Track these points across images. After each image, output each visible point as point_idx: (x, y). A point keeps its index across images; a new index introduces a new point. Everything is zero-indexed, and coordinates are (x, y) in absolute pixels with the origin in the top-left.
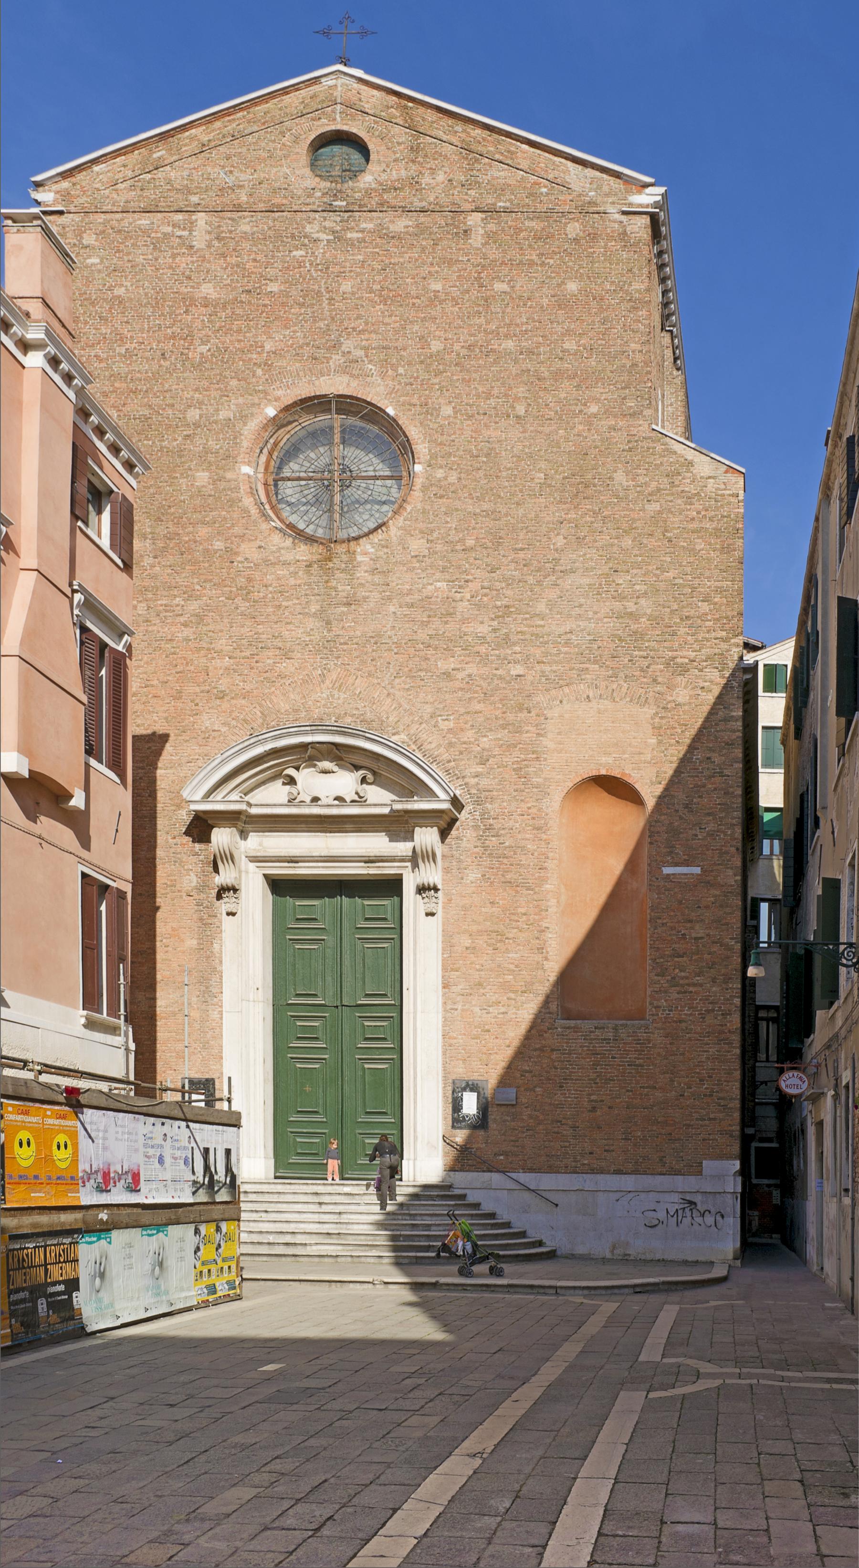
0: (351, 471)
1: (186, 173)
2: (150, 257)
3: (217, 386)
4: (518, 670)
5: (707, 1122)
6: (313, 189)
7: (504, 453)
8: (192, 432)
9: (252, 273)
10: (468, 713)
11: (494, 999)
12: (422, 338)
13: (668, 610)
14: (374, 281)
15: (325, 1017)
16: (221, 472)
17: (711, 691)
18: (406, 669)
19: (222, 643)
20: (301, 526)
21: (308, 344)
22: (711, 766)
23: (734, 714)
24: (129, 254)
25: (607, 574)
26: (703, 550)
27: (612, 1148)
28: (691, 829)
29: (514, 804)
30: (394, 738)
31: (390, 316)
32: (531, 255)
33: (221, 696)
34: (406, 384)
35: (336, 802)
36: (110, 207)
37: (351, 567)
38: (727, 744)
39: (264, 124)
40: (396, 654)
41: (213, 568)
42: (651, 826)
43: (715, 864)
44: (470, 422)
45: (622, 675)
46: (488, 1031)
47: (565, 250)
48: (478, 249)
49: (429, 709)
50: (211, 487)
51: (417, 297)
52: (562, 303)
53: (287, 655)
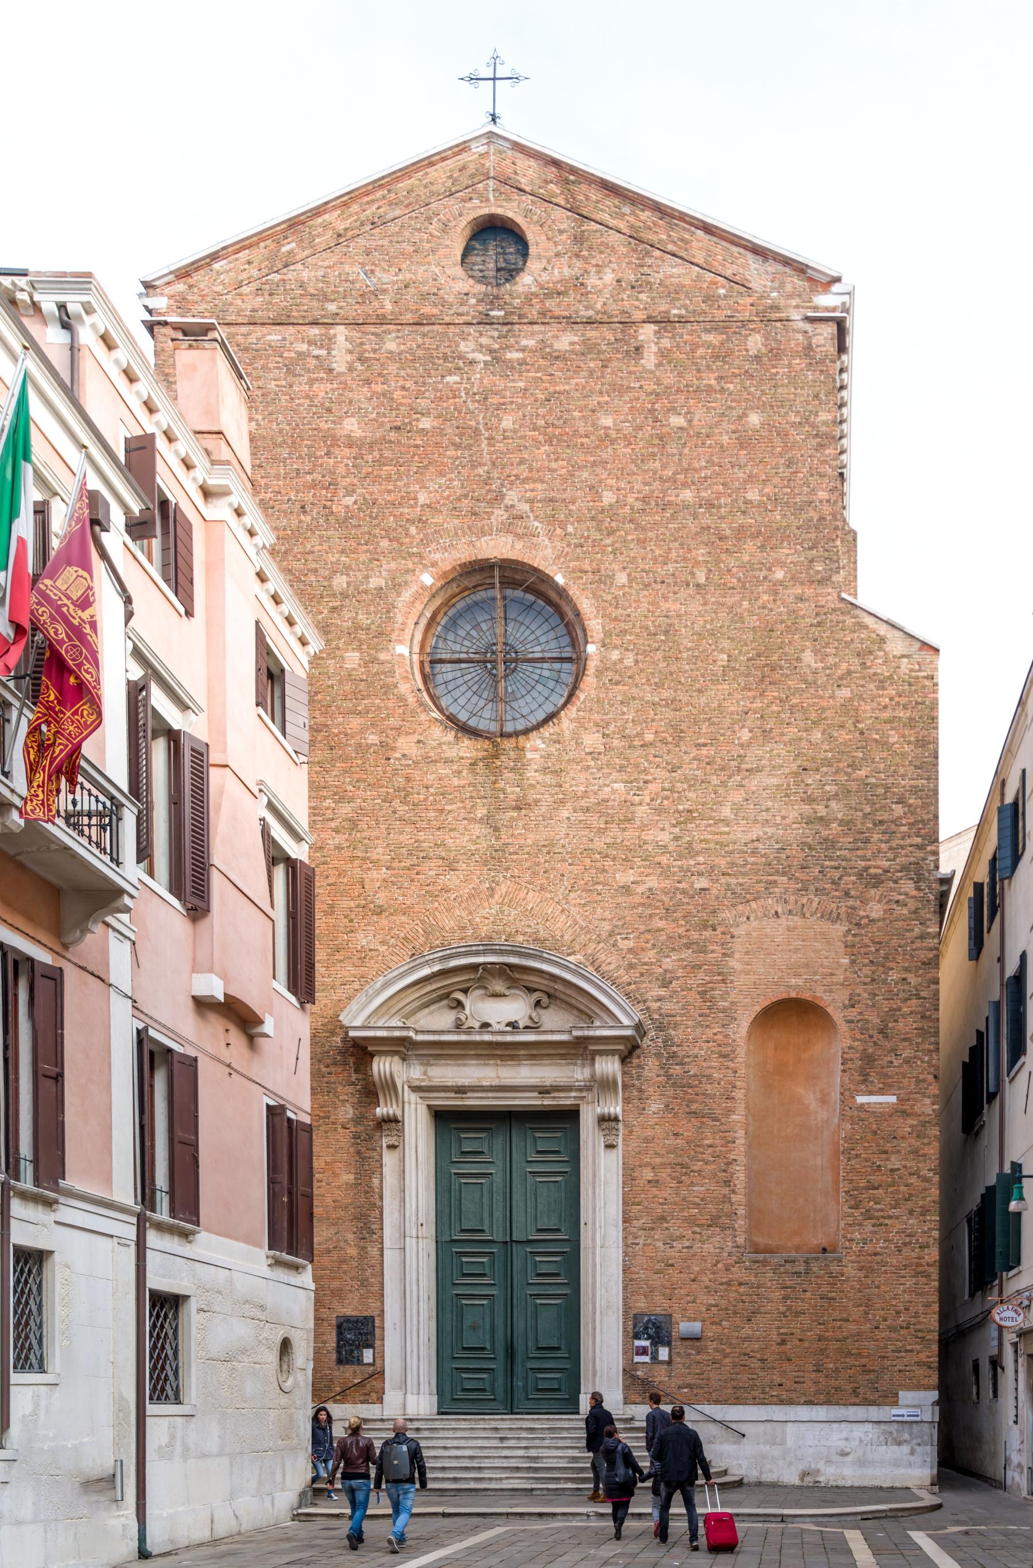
0: (516, 652)
1: (320, 273)
2: (284, 383)
3: (365, 547)
4: (702, 883)
5: (903, 1354)
6: (467, 294)
7: (683, 630)
8: (339, 603)
9: (401, 404)
10: (649, 931)
11: (678, 1233)
12: (592, 488)
13: (860, 814)
14: (538, 415)
15: (492, 1253)
16: (373, 652)
17: (906, 905)
18: (582, 882)
19: (379, 853)
20: (463, 716)
21: (466, 496)
22: (906, 987)
23: (930, 930)
24: (258, 378)
25: (796, 773)
26: (896, 743)
27: (802, 1380)
28: (886, 1056)
29: (699, 1030)
30: (570, 958)
31: (556, 460)
32: (709, 379)
33: (379, 911)
34: (576, 546)
35: (509, 1029)
36: (234, 318)
37: (519, 767)
38: (924, 963)
39: (407, 206)
40: (570, 865)
41: (367, 765)
42: (844, 1053)
43: (911, 1093)
44: (646, 593)
45: (812, 888)
46: (672, 1265)
47: (746, 372)
48: (651, 372)
49: (607, 926)
50: (363, 670)
51: (586, 436)
52: (744, 440)
53: (451, 866)
